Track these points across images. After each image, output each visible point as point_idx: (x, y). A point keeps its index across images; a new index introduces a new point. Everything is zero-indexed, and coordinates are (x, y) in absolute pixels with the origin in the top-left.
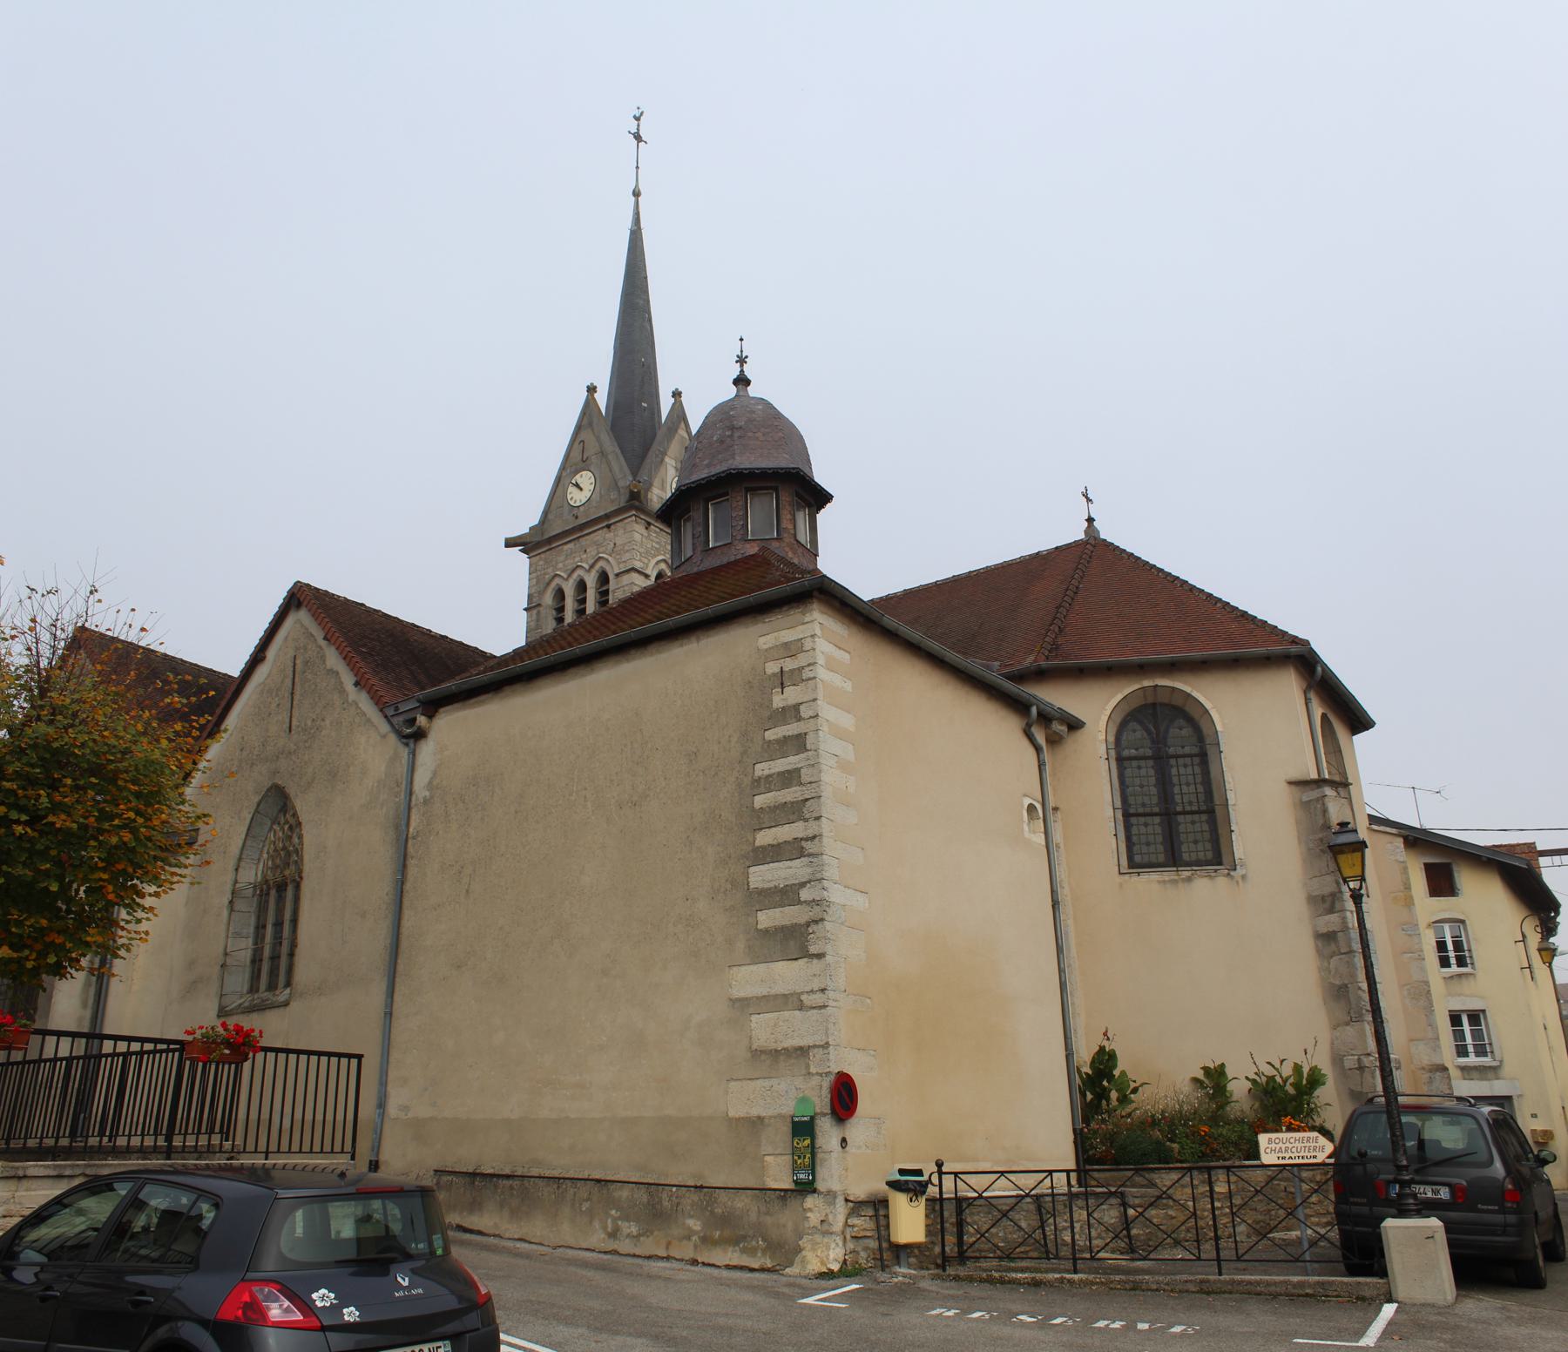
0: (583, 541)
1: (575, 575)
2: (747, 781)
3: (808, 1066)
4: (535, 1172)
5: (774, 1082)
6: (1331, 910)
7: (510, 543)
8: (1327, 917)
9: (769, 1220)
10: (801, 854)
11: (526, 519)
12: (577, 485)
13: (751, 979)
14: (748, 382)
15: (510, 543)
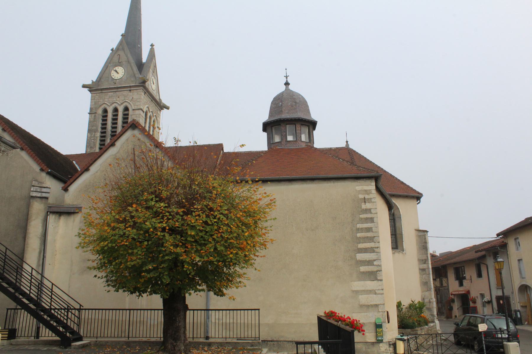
0: (118, 93)
2: (354, 229)
4: (282, 339)
6: (425, 263)
7: (84, 86)
9: (369, 350)
10: (374, 252)
11: (92, 77)
12: (116, 71)
13: (358, 285)
15: (84, 86)
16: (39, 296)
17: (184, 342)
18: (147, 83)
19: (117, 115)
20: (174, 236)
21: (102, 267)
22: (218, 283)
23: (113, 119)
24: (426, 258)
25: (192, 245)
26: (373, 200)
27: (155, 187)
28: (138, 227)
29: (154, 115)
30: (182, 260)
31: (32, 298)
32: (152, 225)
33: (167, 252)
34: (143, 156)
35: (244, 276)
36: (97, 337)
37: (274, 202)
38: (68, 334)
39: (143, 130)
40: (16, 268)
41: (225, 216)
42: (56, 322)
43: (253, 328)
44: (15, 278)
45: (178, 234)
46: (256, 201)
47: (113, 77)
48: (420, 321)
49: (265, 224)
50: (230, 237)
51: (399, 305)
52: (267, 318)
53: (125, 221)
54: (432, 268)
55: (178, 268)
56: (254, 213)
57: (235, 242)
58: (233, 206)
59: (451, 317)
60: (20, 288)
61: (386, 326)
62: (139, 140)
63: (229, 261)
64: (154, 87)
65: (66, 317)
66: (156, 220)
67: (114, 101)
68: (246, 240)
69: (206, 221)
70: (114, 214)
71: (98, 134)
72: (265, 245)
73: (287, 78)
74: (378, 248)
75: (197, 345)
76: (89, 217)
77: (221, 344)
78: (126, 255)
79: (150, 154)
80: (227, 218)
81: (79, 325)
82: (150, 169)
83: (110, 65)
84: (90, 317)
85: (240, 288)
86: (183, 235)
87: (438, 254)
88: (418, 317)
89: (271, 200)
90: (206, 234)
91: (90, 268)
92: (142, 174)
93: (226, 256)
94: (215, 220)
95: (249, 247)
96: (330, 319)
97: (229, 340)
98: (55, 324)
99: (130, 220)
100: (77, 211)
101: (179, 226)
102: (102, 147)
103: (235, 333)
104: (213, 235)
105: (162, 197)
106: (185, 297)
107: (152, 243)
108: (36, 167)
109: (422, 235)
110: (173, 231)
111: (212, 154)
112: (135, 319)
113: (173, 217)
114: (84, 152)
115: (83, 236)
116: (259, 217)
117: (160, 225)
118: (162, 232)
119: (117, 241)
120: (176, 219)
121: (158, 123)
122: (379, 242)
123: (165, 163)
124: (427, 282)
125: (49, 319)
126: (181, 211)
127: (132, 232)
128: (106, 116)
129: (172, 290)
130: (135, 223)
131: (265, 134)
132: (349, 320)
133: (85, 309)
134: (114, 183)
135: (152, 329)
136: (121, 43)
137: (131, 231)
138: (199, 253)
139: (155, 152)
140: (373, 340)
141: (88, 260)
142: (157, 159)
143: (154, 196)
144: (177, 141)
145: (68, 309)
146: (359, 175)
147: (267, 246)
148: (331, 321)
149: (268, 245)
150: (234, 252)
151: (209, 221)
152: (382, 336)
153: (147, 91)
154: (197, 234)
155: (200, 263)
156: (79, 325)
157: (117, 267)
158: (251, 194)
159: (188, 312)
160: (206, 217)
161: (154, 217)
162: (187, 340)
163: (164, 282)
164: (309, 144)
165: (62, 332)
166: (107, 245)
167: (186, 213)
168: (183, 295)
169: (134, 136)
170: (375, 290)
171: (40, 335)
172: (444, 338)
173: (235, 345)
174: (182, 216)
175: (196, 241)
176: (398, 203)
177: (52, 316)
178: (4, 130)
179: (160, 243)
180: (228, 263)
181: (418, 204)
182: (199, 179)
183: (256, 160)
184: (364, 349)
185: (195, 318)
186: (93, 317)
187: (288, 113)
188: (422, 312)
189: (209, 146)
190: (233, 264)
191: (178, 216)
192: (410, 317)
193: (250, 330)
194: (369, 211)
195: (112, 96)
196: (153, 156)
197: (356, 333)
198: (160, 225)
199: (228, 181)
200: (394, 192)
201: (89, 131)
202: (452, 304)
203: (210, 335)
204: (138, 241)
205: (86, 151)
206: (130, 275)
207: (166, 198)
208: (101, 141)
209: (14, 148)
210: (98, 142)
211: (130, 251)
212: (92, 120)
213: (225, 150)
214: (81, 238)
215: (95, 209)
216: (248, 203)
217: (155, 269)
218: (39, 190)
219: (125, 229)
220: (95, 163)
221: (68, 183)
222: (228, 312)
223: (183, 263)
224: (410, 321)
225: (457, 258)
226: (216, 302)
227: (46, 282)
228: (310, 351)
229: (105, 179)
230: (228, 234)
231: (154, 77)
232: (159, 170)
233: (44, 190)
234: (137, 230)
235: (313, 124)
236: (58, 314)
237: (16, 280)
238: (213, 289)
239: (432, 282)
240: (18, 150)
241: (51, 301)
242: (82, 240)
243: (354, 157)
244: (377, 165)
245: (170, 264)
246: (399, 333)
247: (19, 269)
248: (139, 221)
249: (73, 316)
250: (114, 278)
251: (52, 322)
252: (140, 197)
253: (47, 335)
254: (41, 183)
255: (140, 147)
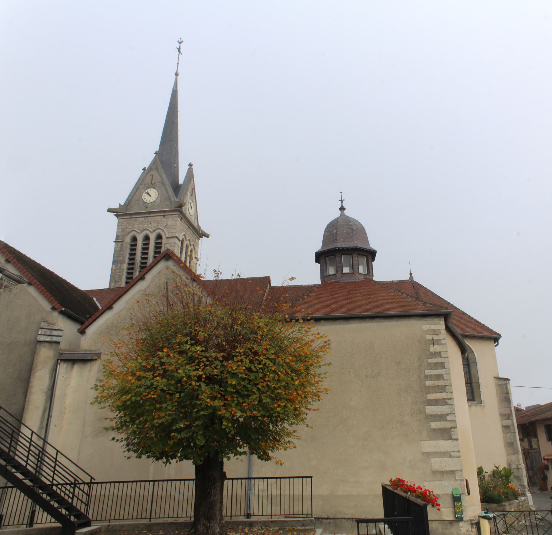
0: (149, 219)
1: (144, 233)
2: (422, 376)
3: (455, 477)
4: (339, 516)
5: (442, 482)
6: (508, 419)
7: (110, 210)
8: (507, 421)
9: (447, 531)
10: (446, 404)
11: (119, 199)
12: (148, 194)
13: (430, 446)
14: (344, 209)
15: (110, 210)
16: (38, 468)
17: (220, 522)
18: (183, 208)
19: (148, 244)
20: (211, 386)
21: (122, 427)
22: (263, 444)
23: (143, 249)
24: (509, 412)
25: (232, 397)
26: (443, 342)
27: (191, 327)
28: (169, 376)
29: (192, 243)
30: (220, 415)
31: (29, 471)
32: (186, 373)
33: (203, 406)
34: (178, 292)
35: (294, 434)
36: (110, 520)
37: (329, 345)
38: (72, 518)
39: (178, 261)
40: (11, 432)
41: (271, 362)
42: (58, 502)
43: (305, 502)
44: (8, 446)
45: (216, 383)
46: (307, 343)
47: (145, 201)
48: (507, 493)
49: (318, 371)
50: (277, 386)
51: (480, 471)
52: (321, 489)
53: (153, 369)
54: (518, 425)
55: (215, 426)
56: (306, 357)
57: (284, 393)
58: (281, 350)
59: (546, 490)
60: (13, 459)
61: (465, 499)
62: (173, 272)
63: (276, 416)
64: (192, 212)
65: (71, 495)
66: (191, 367)
67: (144, 228)
68: (296, 390)
69: (250, 368)
70: (140, 361)
71: (125, 266)
72: (319, 396)
73: (342, 202)
74: (450, 399)
75: (235, 526)
76: (109, 365)
77: (265, 524)
78: (153, 410)
79: (186, 289)
80: (274, 364)
81: (87, 505)
82: (185, 306)
83: (141, 187)
84: (103, 493)
85: (288, 449)
86: (223, 385)
87: (523, 407)
88: (505, 488)
89: (325, 342)
90: (249, 384)
91: (107, 429)
92: (176, 312)
93: (272, 409)
94: (260, 366)
95: (299, 398)
96: (397, 488)
97: (275, 518)
98: (56, 505)
99: (160, 368)
100: (95, 358)
101: (218, 370)
102: (129, 281)
103: (283, 508)
104: (258, 384)
105: (198, 339)
106: (222, 463)
107: (185, 396)
108: (46, 305)
109: (503, 384)
110: (210, 380)
111: (258, 288)
112: (160, 494)
113: (211, 363)
114: (108, 287)
115: (100, 389)
116: (311, 361)
117: (195, 373)
118: (197, 381)
119: (142, 393)
120: (215, 365)
121: (196, 253)
122: (452, 392)
123: (203, 299)
124: (513, 443)
125: (48, 498)
126: (220, 355)
127: (161, 382)
128: (136, 245)
129: (207, 454)
130: (165, 371)
131: (318, 265)
132: (420, 491)
133: (98, 483)
134: (142, 324)
135: (181, 506)
136: (154, 162)
137: (160, 381)
138: (241, 406)
139: (191, 287)
140: (451, 518)
141: (106, 419)
142: (194, 294)
143: (189, 338)
144: (217, 273)
145: (75, 484)
146: (426, 312)
147: (321, 397)
148: (399, 492)
149: (322, 395)
150: (282, 404)
151: (253, 368)
152: (462, 513)
153: (184, 217)
154: (239, 384)
155: (241, 420)
156: (87, 505)
157: (141, 426)
158: (302, 335)
159: (226, 481)
160: (250, 363)
161: (188, 364)
162: (223, 520)
163: (198, 443)
164: (368, 277)
165: (64, 516)
166: (130, 399)
167: (226, 359)
168: (220, 460)
169: (167, 268)
170: (449, 453)
171: (35, 522)
172: (540, 517)
173: (282, 525)
174: (221, 362)
175: (237, 392)
176: (473, 345)
177: (53, 495)
178: (8, 261)
179: (194, 395)
180: (275, 418)
181: (496, 346)
182: (242, 318)
183: (307, 295)
184: (440, 530)
185: (234, 490)
186: (107, 493)
187: (343, 241)
188: (509, 482)
189: (254, 280)
190: (281, 419)
191: (217, 362)
192: (495, 487)
193: (300, 503)
194: (438, 354)
195: (143, 222)
196: (189, 291)
197: (429, 507)
198: (195, 373)
199: (276, 320)
200: (467, 333)
201: (114, 262)
202: (545, 472)
203: (251, 512)
204: (168, 393)
205: (110, 286)
206: (156, 437)
207: (204, 341)
208: (128, 273)
209: (19, 282)
210: (125, 275)
211: (158, 406)
212: (118, 249)
213: (273, 284)
214: (98, 391)
215: (117, 355)
216: (299, 345)
217: (187, 427)
218: (48, 333)
219: (153, 379)
220: (120, 300)
221: (86, 324)
222: (274, 480)
223: (221, 420)
224: (495, 493)
225: (548, 413)
226: (261, 468)
227: (49, 449)
228: (374, 532)
229: (131, 319)
230: (275, 382)
231: (193, 201)
232: (196, 307)
233: (55, 333)
234: (168, 380)
235: (371, 254)
236: (61, 491)
237: (9, 449)
238: (256, 451)
239: (519, 443)
240: (25, 285)
241: (54, 473)
242: (100, 393)
243: (420, 291)
244: (446, 301)
245: (206, 421)
246: (483, 509)
247: (14, 435)
248: (170, 368)
249: (81, 493)
250: (136, 441)
251: (52, 503)
252: (173, 339)
253: (44, 521)
254: (52, 324)
255: (174, 280)
